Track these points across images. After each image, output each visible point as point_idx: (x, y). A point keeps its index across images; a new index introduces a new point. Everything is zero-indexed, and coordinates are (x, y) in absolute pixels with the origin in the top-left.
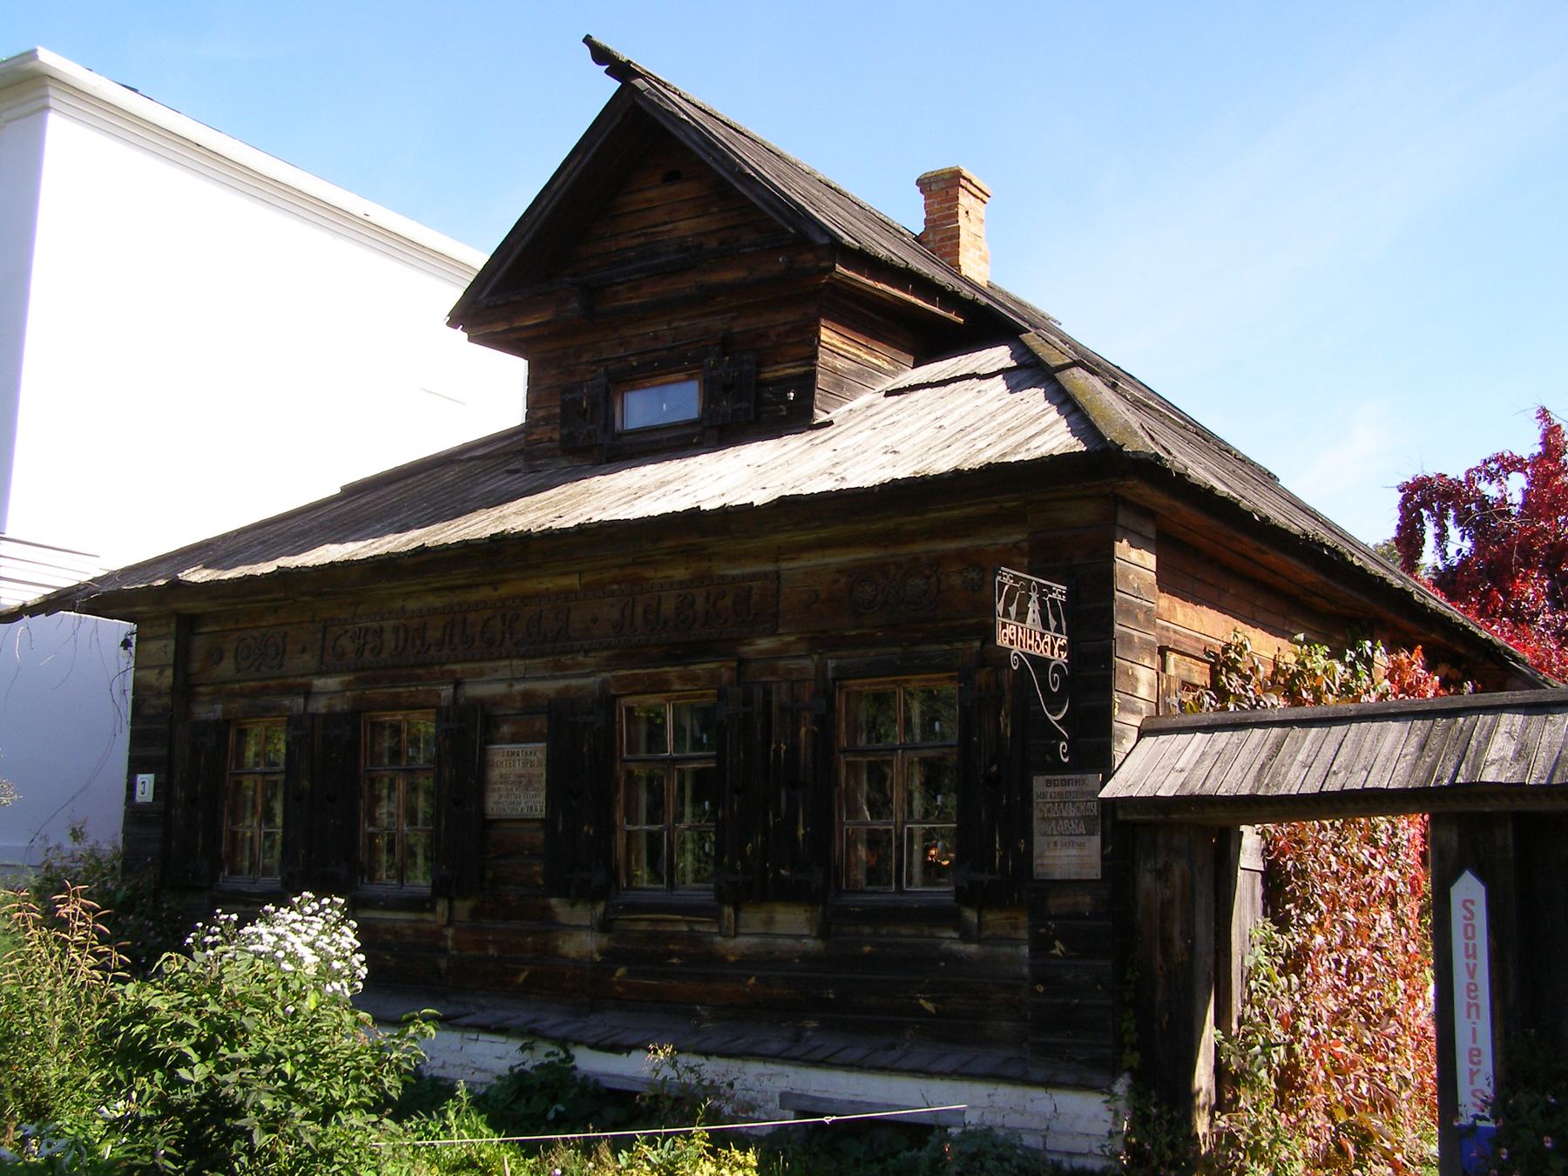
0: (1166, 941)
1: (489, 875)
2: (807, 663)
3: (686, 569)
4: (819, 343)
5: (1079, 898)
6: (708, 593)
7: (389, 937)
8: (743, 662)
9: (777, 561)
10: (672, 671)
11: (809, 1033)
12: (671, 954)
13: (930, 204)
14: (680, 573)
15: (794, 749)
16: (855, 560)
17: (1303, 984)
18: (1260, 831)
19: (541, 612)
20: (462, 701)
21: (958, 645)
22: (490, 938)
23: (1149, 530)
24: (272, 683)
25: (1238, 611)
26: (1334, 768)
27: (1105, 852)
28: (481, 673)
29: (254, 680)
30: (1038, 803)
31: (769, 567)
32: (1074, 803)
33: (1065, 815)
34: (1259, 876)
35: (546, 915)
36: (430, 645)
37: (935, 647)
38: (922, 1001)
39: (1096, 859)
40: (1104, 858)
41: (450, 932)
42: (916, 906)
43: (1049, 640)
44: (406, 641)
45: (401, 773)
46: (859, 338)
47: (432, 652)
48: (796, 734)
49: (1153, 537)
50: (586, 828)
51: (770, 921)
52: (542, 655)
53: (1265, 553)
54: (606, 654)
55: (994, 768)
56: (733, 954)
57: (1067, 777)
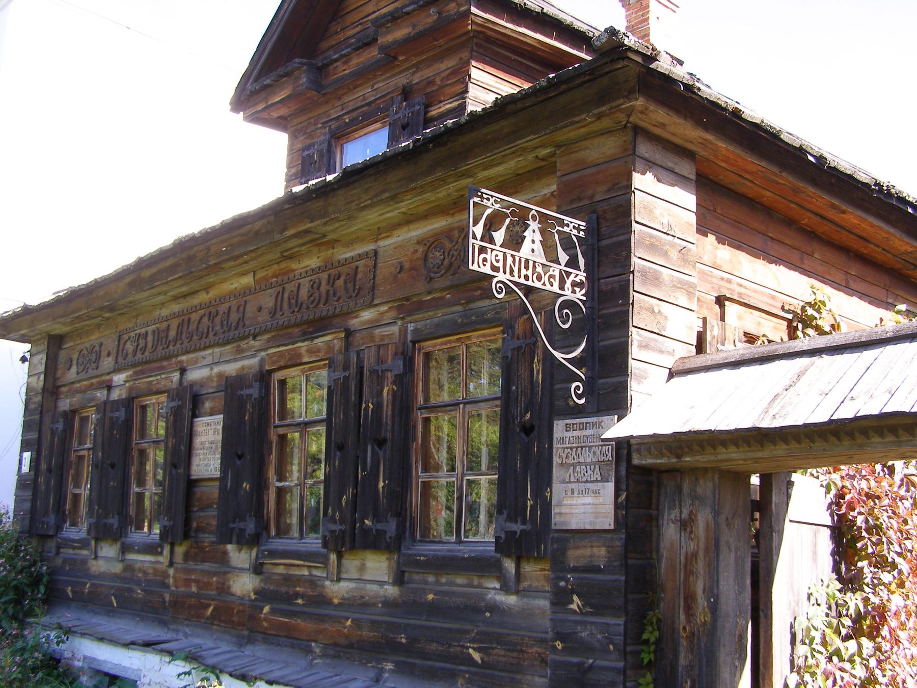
0: (690, 598)
1: (194, 525)
2: (395, 329)
4: (469, 80)
5: (595, 550)
6: (329, 275)
7: (140, 575)
8: (349, 333)
10: (303, 346)
11: (386, 675)
12: (297, 595)
13: (629, 15)
14: (313, 262)
15: (378, 406)
16: (431, 230)
17: (878, 648)
18: (825, 483)
19: (230, 307)
20: (185, 384)
22: (193, 577)
23: (687, 169)
24: (94, 381)
25: (826, 276)
26: (852, 394)
27: (620, 500)
29: (85, 380)
30: (557, 448)
32: (590, 447)
33: (581, 460)
34: (827, 532)
35: (224, 558)
38: (471, 651)
39: (610, 508)
40: (617, 506)
41: (171, 571)
42: (466, 556)
43: (557, 273)
44: (158, 340)
46: (514, 79)
49: (693, 177)
50: (244, 485)
51: (362, 568)
53: (844, 212)
55: (528, 416)
56: (336, 597)
57: (584, 420)
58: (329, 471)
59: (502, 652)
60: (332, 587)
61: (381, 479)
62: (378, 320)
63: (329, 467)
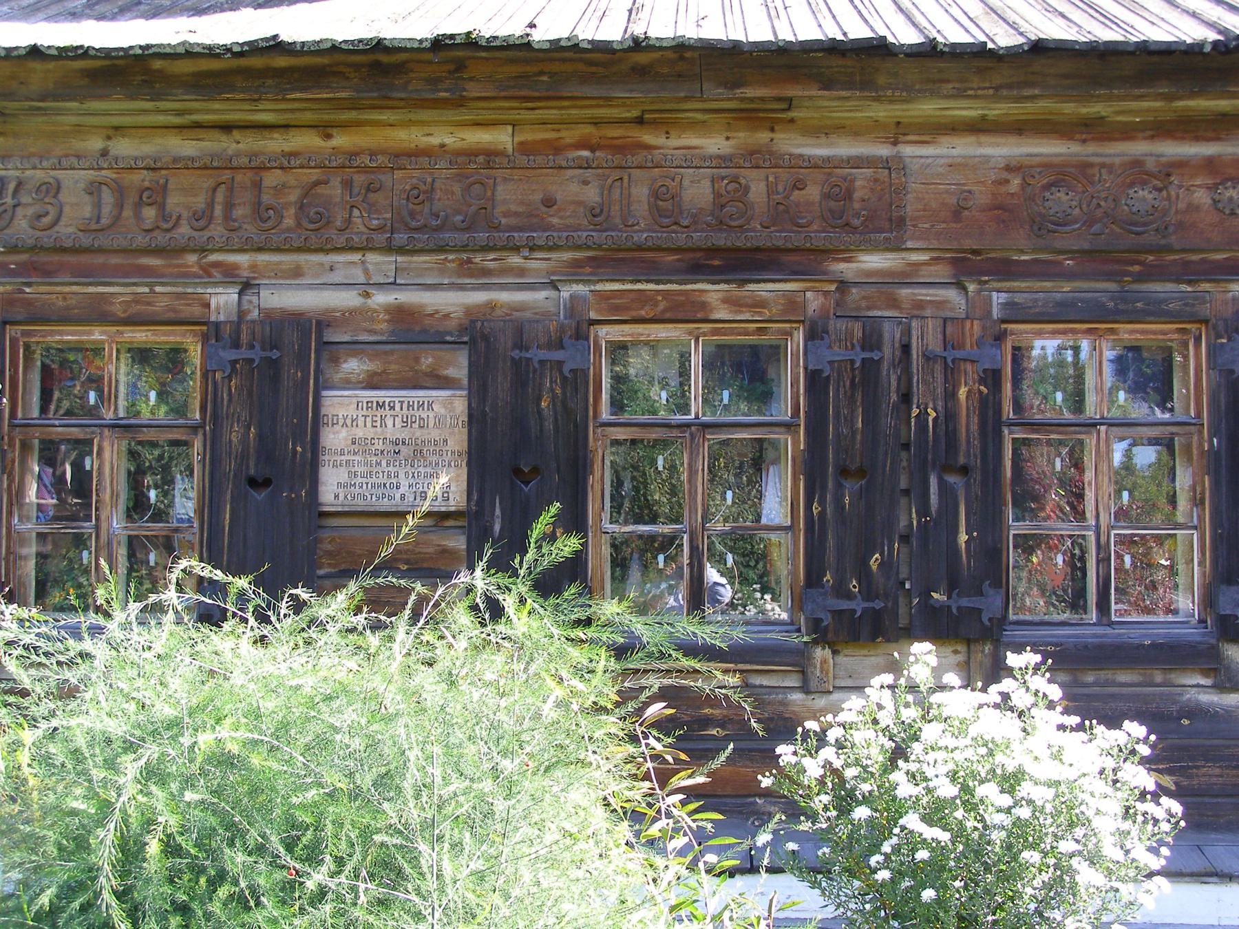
3: (728, 138)
9: (895, 143)
10: (713, 292)
15: (950, 416)
21: (1206, 286)
28: (297, 272)
31: (884, 151)
36: (179, 217)
37: (1170, 286)
45: (106, 430)
47: (184, 230)
48: (951, 395)
52: (441, 249)
54: (567, 256)
58: (822, 514)
59: (1217, 771)
60: (810, 703)
61: (962, 528)
62: (904, 274)
63: (822, 503)
